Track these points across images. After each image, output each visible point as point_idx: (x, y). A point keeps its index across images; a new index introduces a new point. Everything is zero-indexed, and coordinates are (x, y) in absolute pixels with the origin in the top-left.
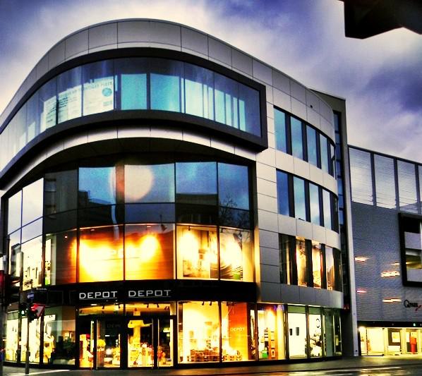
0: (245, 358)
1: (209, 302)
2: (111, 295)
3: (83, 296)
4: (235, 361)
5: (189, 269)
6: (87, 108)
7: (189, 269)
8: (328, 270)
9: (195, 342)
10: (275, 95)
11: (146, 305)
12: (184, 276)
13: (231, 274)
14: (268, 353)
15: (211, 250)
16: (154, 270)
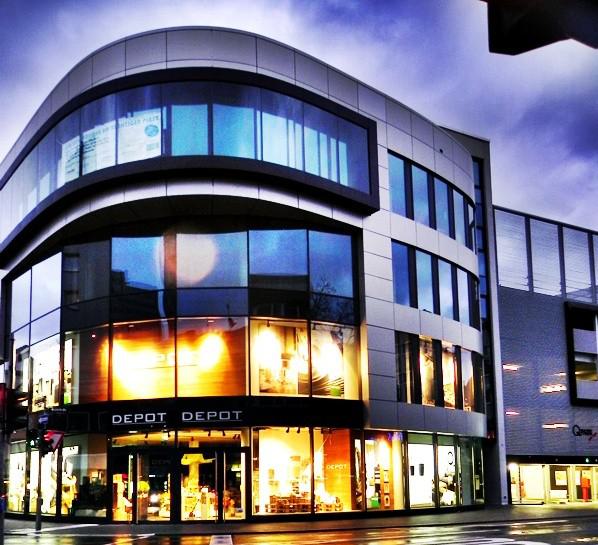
0: (347, 508)
1: (297, 429)
2: (158, 418)
3: (117, 419)
4: (333, 511)
7: (267, 381)
11: (207, 433)
12: (261, 391)
13: (328, 388)
14: (379, 501)
15: (299, 354)
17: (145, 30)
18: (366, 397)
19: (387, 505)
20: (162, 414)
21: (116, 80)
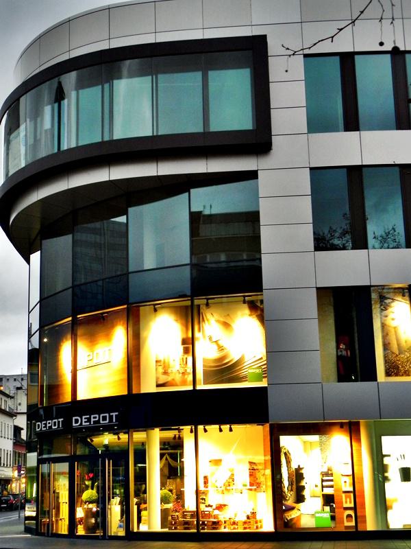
2: (111, 417)
4: (240, 530)
5: (165, 373)
7: (165, 373)
9: (327, 474)
10: (19, 62)
11: (116, 437)
13: (243, 373)
14: (333, 518)
15: (204, 336)
16: (121, 380)
20: (114, 414)
21: (35, 75)
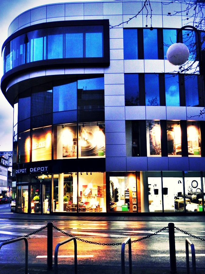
0: (104, 210)
1: (90, 173)
3: (32, 170)
4: (94, 212)
6: (122, 118)
7: (66, 152)
8: (152, 225)
12: (64, 157)
13: (96, 153)
17: (35, 7)
18: (189, 156)
19: (134, 210)
20: (46, 167)
